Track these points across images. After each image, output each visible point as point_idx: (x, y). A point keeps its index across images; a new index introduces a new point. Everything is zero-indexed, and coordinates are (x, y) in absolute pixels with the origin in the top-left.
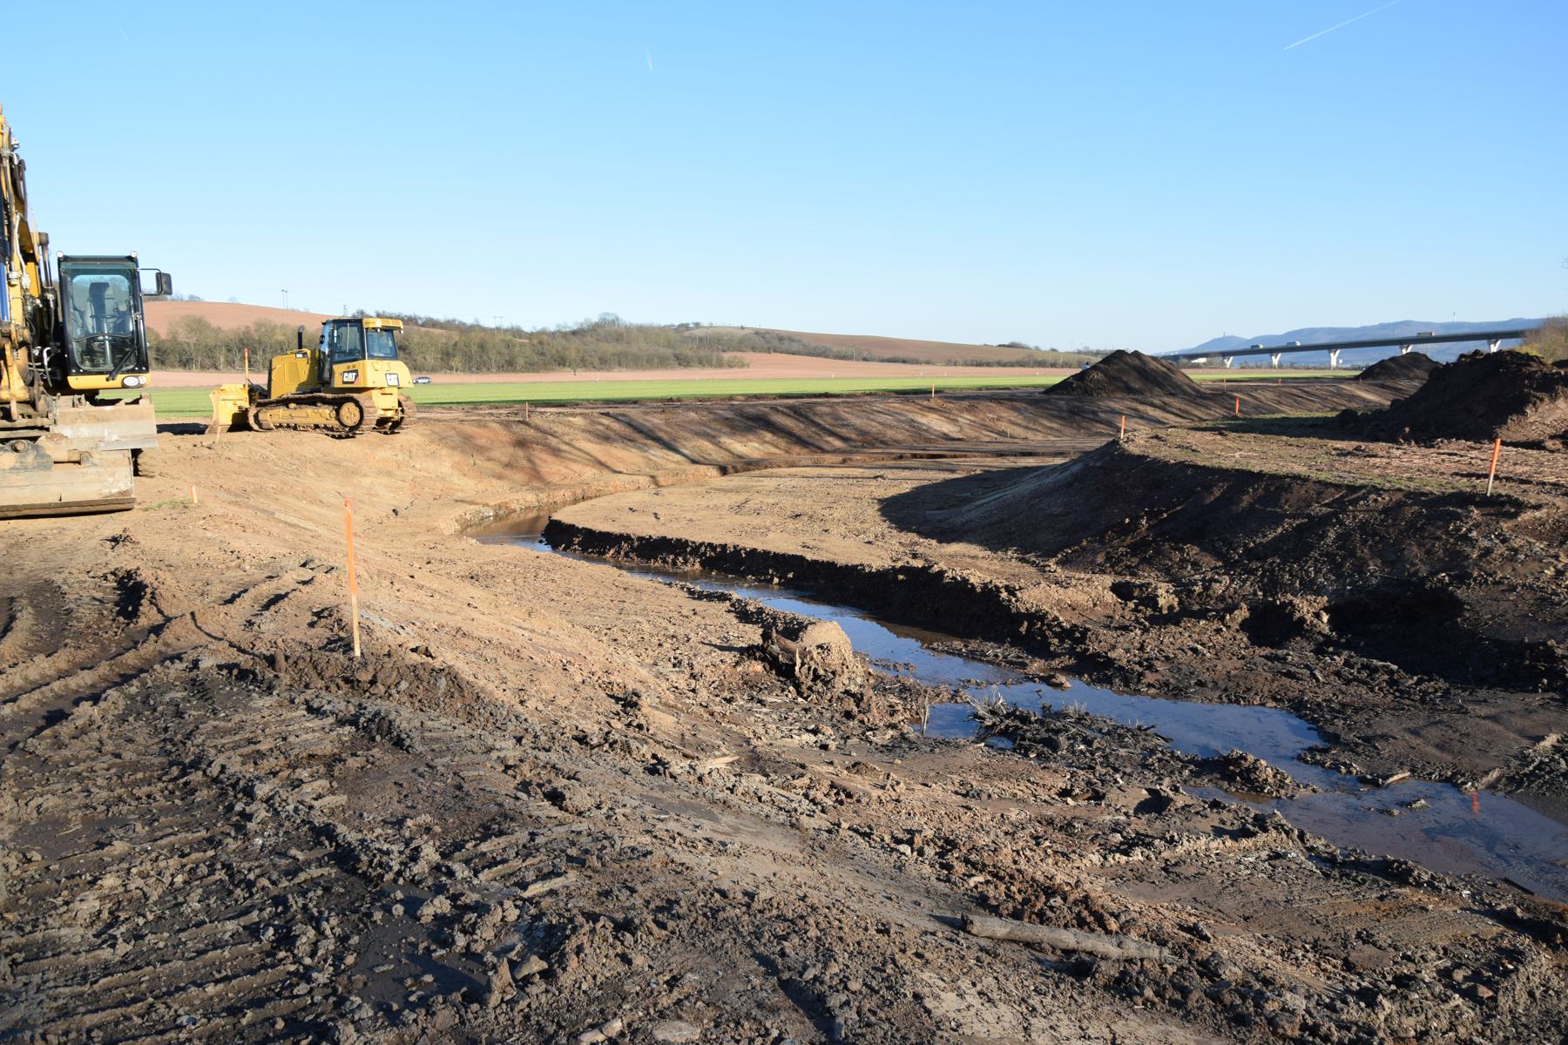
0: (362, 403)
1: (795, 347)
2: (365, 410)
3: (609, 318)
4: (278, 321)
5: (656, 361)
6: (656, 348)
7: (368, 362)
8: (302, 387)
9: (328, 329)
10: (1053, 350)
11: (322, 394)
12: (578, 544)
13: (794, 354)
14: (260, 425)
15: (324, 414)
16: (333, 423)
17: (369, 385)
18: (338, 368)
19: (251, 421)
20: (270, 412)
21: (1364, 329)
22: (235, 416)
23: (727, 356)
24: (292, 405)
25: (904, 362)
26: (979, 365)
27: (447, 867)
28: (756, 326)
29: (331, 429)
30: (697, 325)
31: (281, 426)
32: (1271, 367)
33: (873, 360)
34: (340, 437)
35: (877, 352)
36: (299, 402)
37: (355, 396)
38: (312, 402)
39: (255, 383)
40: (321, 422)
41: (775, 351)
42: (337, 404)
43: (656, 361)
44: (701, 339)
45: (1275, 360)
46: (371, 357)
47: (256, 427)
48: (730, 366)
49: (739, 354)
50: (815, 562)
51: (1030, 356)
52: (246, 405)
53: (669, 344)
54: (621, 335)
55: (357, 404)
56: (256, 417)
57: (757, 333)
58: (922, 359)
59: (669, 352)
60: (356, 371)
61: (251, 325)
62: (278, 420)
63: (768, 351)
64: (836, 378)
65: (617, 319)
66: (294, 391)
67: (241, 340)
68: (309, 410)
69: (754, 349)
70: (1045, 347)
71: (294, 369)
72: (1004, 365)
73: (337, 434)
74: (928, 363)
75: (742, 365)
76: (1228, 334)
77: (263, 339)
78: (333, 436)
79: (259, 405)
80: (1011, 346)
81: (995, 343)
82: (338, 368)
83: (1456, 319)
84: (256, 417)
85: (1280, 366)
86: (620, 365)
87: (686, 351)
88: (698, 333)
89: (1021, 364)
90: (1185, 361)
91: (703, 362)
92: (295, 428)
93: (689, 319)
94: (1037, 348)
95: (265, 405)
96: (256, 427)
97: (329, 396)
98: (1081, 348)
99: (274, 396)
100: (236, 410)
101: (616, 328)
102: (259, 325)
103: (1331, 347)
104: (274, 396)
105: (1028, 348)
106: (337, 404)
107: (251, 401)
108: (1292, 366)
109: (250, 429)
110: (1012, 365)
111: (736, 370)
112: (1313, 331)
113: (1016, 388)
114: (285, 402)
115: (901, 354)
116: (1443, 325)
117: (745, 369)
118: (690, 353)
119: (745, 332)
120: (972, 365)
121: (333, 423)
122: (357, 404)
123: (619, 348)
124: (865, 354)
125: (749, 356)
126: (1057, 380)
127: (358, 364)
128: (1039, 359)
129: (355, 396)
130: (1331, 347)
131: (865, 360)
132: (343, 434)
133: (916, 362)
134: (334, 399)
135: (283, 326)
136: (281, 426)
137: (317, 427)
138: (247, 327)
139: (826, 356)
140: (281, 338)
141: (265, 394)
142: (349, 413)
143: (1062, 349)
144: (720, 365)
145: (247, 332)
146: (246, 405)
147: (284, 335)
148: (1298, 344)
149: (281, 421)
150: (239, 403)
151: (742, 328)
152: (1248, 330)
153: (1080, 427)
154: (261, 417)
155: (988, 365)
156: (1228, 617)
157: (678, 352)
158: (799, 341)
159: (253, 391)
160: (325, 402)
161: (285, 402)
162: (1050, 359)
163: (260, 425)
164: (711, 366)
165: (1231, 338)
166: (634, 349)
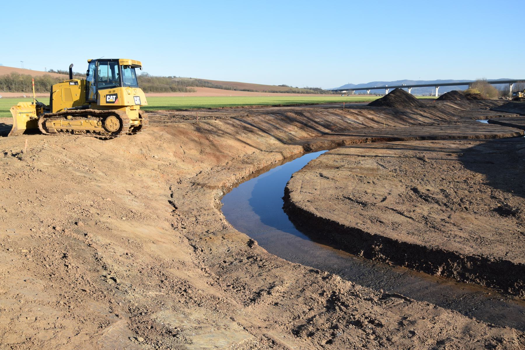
0: (122, 117)
1: (210, 85)
2: (124, 121)
3: (145, 74)
4: (21, 73)
5: (164, 89)
6: (163, 85)
7: (123, 88)
8: (76, 104)
9: (93, 66)
11: (91, 110)
12: (381, 251)
13: (210, 87)
14: (47, 130)
15: (93, 123)
16: (100, 129)
17: (126, 105)
18: (102, 93)
19: (41, 127)
20: (54, 122)
21: (392, 82)
22: (28, 123)
23: (188, 88)
24: (70, 117)
25: (248, 91)
26: (274, 92)
28: (196, 78)
29: (99, 133)
30: (175, 77)
31: (62, 131)
32: (367, 94)
34: (106, 139)
35: (224, 86)
36: (74, 115)
37: (116, 111)
38: (85, 115)
39: (40, 101)
40: (91, 129)
41: (204, 87)
42: (103, 117)
43: (164, 89)
44: (178, 82)
45: (368, 92)
46: (125, 85)
47: (44, 131)
48: (190, 92)
49: (192, 87)
51: (291, 89)
52: (35, 116)
53: (167, 84)
54: (150, 80)
55: (118, 117)
56: (44, 124)
57: (196, 80)
59: (168, 86)
60: (116, 95)
61: (9, 74)
62: (59, 127)
63: (202, 86)
64: (232, 97)
65: (148, 74)
66: (70, 107)
67: (6, 80)
68: (82, 120)
69: (197, 86)
70: (294, 86)
71: (69, 93)
73: (103, 137)
74: (256, 91)
75: (194, 91)
76: (350, 83)
77: (15, 80)
78: (101, 139)
79: (46, 116)
80: (283, 86)
82: (102, 93)
84: (44, 124)
85: (371, 94)
86: (151, 91)
87: (174, 86)
88: (177, 80)
89: (288, 92)
90: (340, 92)
91: (180, 90)
92: (72, 132)
93: (172, 75)
94: (291, 87)
95: (50, 116)
96: (44, 131)
97: (97, 111)
98: (306, 87)
99: (54, 111)
100: (29, 119)
101: (147, 77)
102: (13, 74)
103: (436, 85)
104: (54, 111)
105: (288, 87)
106: (103, 117)
107: (38, 114)
109: (40, 133)
110: (285, 92)
111: (192, 93)
112: (376, 83)
113: (350, 102)
114: (65, 115)
115: (247, 88)
116: (417, 82)
117: (195, 93)
118: (176, 87)
119: (192, 80)
120: (271, 92)
121: (100, 129)
122: (118, 117)
123: (150, 85)
125: (196, 88)
126: (374, 98)
127: (117, 90)
128: (294, 90)
129: (116, 111)
131: (235, 90)
132: (108, 137)
133: (252, 91)
134: (82, 112)
135: (22, 75)
136: (62, 131)
137: (88, 132)
138: (8, 75)
139: (222, 89)
140: (22, 79)
141: (49, 108)
142: (112, 123)
143: (299, 87)
144: (186, 91)
145: (8, 77)
146: (35, 116)
147: (23, 78)
148: (387, 86)
149: (62, 128)
150: (30, 115)
151: (191, 78)
152: (357, 82)
154: (48, 124)
155: (277, 92)
156: (514, 209)
157: (171, 86)
158: (211, 83)
159: (39, 106)
160: (94, 115)
161: (65, 115)
162: (296, 90)
163: (47, 130)
164: (183, 91)
165: (351, 84)
166: (155, 85)
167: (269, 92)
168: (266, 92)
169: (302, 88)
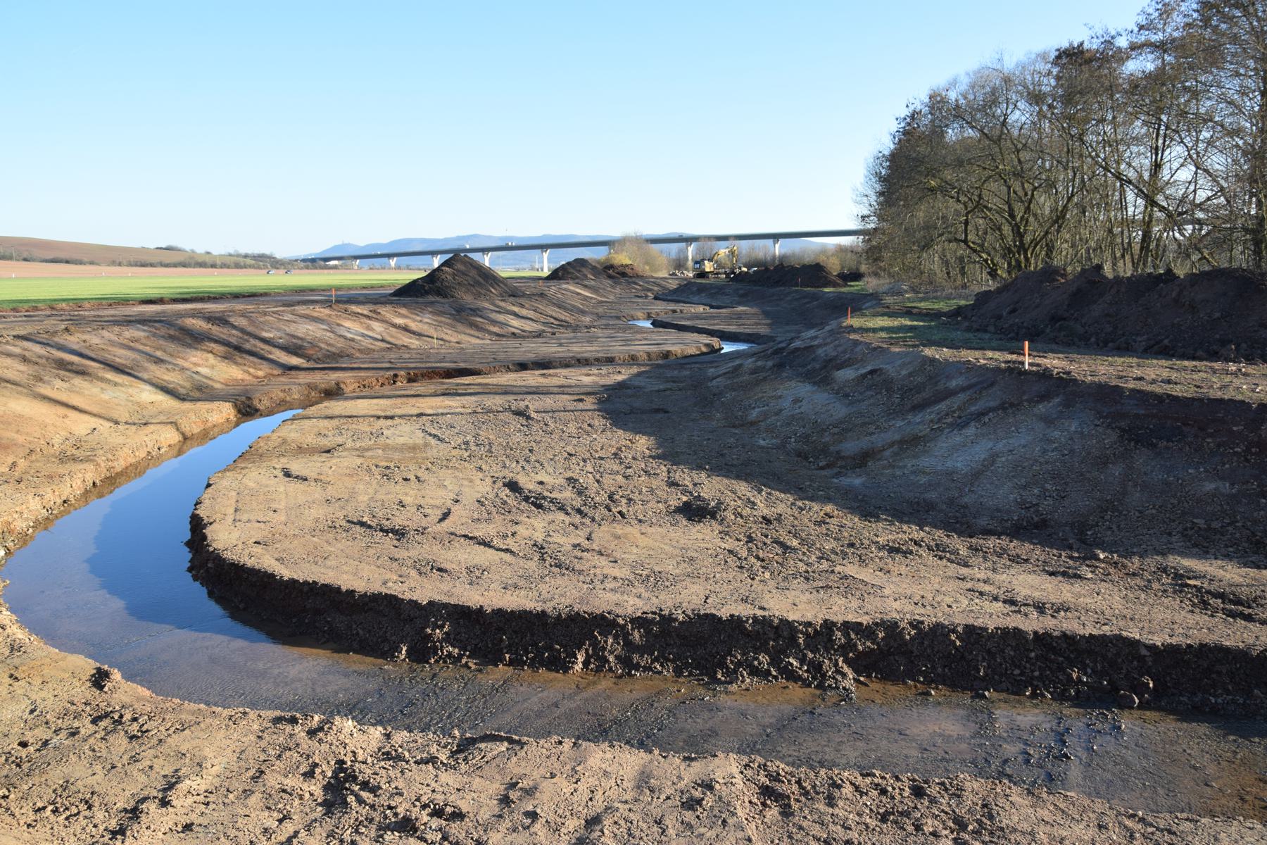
10: (208, 253)
21: (446, 240)
25: (67, 262)
26: (143, 265)
27: (1122, 563)
32: (390, 268)
33: (34, 260)
35: (37, 253)
50: (293, 582)
51: (192, 258)
58: (86, 260)
64: (17, 278)
70: (200, 249)
72: (167, 266)
74: (92, 263)
76: (346, 242)
81: (153, 246)
83: (595, 234)
89: (184, 265)
90: (322, 263)
94: (193, 251)
98: (232, 252)
105: (184, 251)
108: (408, 268)
110: (175, 265)
124: (25, 255)
130: (390, 256)
131: (25, 260)
133: (81, 263)
143: (215, 252)
148: (468, 247)
153: (757, 263)
155: (152, 265)
167: (130, 265)
168: (120, 264)
169: (223, 253)
